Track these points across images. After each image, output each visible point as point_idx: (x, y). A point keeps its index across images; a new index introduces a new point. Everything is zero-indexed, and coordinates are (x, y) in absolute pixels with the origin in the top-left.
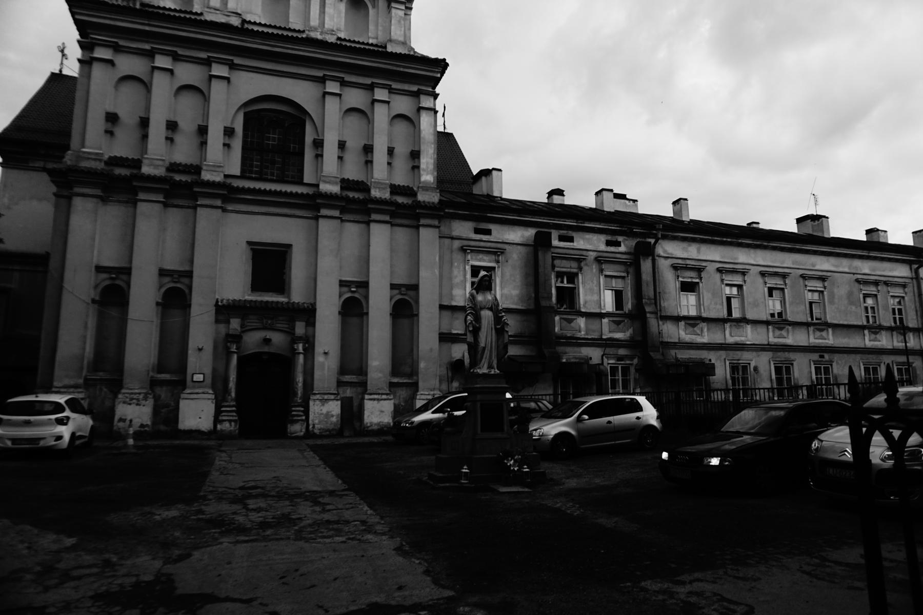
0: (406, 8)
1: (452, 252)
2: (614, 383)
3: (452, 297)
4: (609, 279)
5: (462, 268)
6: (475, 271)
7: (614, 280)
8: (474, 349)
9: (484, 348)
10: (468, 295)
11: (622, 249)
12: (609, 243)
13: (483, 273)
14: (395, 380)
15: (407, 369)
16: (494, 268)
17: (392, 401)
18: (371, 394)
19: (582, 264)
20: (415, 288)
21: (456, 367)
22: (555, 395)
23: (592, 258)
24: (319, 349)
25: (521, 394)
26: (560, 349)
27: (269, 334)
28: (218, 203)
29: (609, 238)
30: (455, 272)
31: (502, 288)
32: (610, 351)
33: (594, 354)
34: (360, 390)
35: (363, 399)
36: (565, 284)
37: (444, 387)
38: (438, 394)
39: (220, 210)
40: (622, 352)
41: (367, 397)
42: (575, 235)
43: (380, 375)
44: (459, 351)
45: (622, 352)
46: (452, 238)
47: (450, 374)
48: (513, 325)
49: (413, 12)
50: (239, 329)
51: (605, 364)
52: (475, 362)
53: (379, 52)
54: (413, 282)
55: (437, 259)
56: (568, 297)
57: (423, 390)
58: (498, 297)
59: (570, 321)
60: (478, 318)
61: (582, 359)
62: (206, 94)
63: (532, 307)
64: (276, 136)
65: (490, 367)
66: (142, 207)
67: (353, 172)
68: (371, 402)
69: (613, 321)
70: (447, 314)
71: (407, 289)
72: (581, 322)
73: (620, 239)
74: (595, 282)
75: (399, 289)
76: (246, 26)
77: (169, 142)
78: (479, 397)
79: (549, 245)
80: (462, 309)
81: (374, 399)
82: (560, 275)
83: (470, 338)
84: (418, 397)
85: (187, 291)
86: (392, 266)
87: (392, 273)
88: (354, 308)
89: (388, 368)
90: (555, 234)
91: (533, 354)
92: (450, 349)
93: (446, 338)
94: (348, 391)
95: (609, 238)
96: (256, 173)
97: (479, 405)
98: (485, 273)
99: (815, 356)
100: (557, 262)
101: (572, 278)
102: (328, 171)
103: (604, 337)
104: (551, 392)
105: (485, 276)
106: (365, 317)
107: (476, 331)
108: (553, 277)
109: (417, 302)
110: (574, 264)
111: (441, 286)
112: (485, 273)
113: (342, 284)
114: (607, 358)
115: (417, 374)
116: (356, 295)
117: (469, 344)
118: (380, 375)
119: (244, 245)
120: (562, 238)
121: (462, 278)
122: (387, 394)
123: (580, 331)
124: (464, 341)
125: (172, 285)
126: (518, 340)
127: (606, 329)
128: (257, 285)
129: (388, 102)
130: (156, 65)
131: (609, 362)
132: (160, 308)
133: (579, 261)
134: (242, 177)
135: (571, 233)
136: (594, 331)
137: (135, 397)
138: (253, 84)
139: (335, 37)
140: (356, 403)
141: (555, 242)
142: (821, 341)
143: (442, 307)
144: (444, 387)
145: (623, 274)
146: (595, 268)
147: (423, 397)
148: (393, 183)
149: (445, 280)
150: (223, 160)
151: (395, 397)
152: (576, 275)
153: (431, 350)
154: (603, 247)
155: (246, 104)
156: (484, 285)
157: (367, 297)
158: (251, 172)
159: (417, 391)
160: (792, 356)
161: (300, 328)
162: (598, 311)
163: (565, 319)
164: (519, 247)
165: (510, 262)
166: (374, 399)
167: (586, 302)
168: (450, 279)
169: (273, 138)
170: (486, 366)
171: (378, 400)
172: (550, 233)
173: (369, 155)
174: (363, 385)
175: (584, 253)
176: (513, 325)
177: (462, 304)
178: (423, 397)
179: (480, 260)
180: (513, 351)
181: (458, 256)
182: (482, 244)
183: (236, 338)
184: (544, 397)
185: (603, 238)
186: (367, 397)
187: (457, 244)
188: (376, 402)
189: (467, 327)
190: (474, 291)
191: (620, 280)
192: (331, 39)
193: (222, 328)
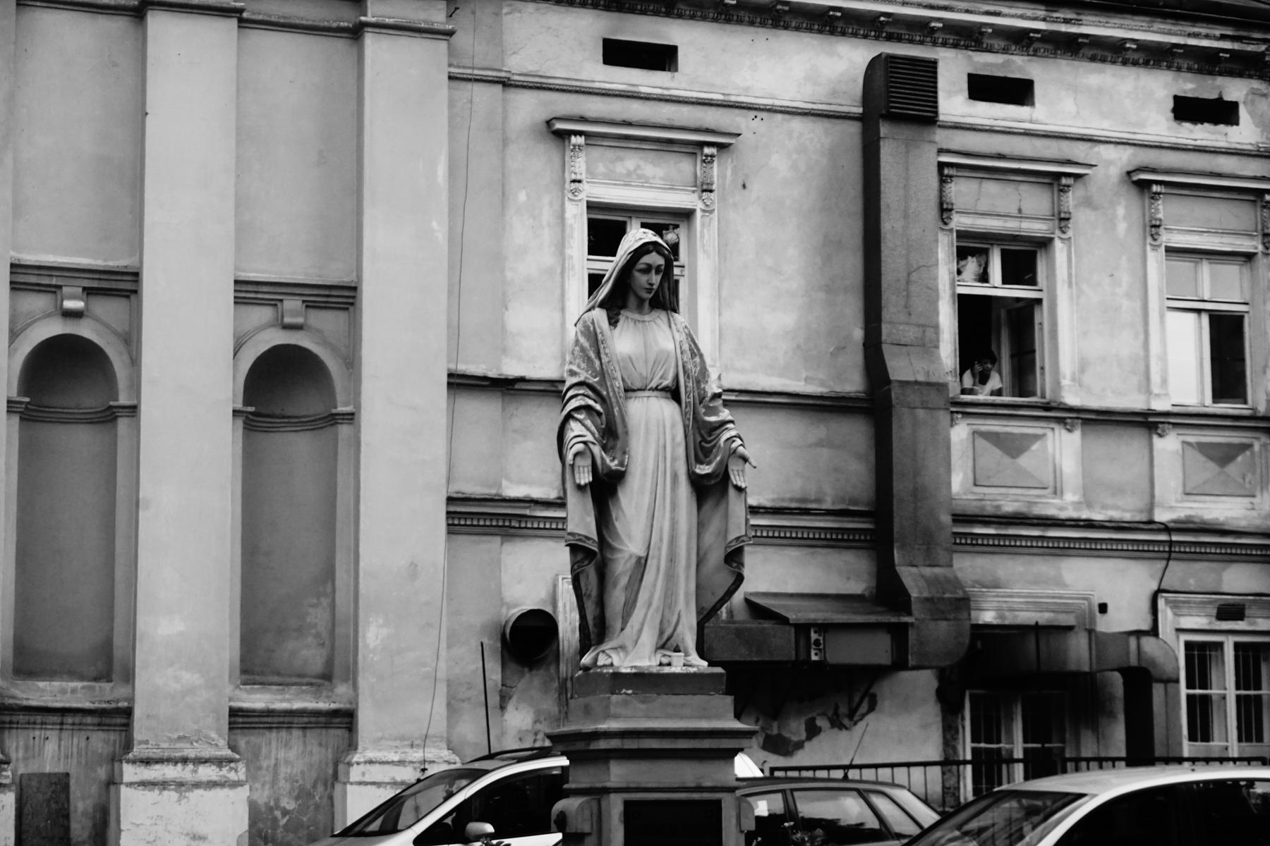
1: (505, 142)
2: (1201, 718)
3: (501, 341)
4: (1184, 266)
5: (547, 215)
6: (604, 234)
7: (1206, 269)
8: (592, 560)
9: (641, 564)
10: (572, 332)
11: (1244, 133)
12: (1186, 110)
13: (636, 236)
14: (257, 700)
15: (311, 656)
16: (686, 215)
17: (243, 793)
18: (147, 762)
19: (1071, 200)
20: (341, 298)
21: (527, 641)
22: (949, 763)
23: (1115, 172)
25: (800, 759)
26: (969, 567)
29: (1190, 86)
30: (519, 230)
31: (722, 302)
32: (1182, 574)
33: (1116, 591)
34: (100, 742)
35: (112, 782)
36: (997, 287)
37: (471, 730)
38: (441, 759)
39: (500, 87)
40: (1239, 579)
41: (130, 772)
42: (1045, 74)
43: (190, 678)
44: (535, 575)
45: (1239, 579)
46: (506, 84)
47: (495, 675)
48: (771, 461)
51: (1166, 629)
52: (595, 631)
54: (335, 274)
55: (442, 170)
56: (1001, 336)
57: (377, 742)
58: (706, 344)
59: (1013, 447)
60: (611, 434)
61: (1066, 609)
63: (853, 383)
65: (667, 644)
68: (151, 795)
69: (1202, 448)
70: (481, 409)
71: (309, 306)
72: (1063, 448)
73: (1234, 89)
74: (1125, 278)
75: (274, 304)
78: (618, 773)
79: (927, 118)
80: (551, 390)
81: (163, 785)
82: (971, 247)
83: (580, 518)
84: (355, 774)
86: (241, 203)
87: (243, 233)
89: (227, 650)
90: (953, 69)
91: (857, 587)
92: (497, 564)
93: (479, 517)
94: (51, 747)
95: (1190, 86)
97: (615, 806)
98: (650, 236)
100: (960, 191)
101: (1023, 259)
103: (1161, 516)
104: (932, 750)
105: (644, 249)
106: (123, 424)
107: (605, 488)
108: (944, 251)
109: (352, 362)
110: (1036, 200)
111: (455, 291)
112: (650, 236)
113: (248, 292)
114: (1175, 605)
115: (351, 675)
116: (85, 330)
117: (578, 550)
118: (190, 678)
120: (982, 88)
121: (548, 259)
122: (220, 762)
123: (1057, 491)
124: (554, 529)
125: (56, 328)
126: (791, 524)
127: (1172, 480)
128: (1220, 392)
131: (1184, 623)
132: (240, 423)
133: (1054, 182)
135: (1018, 65)
136: (1119, 490)
140: (81, 804)
141: (953, 102)
143: (460, 383)
144: (471, 730)
145: (1246, 245)
146: (1125, 213)
147: (377, 773)
149: (470, 261)
151: (252, 777)
152: (1045, 243)
153: (413, 570)
154: (1161, 126)
156: (639, 279)
157: (131, 339)
159: (352, 746)
162: (1133, 402)
163: (987, 436)
164: (797, 124)
165: (755, 187)
166: (163, 785)
167: (1083, 366)
168: (497, 260)
170: (649, 638)
171: (180, 785)
172: (932, 66)
174: (118, 718)
175: (1078, 151)
176: (771, 461)
177: (545, 369)
178: (377, 773)
179: (626, 181)
180: (773, 574)
181: (535, 161)
182: (636, 110)
184: (901, 774)
185: (1162, 86)
186: (130, 772)
187: (528, 109)
188: (171, 795)
189: (567, 469)
190: (600, 316)
191: (1231, 271)
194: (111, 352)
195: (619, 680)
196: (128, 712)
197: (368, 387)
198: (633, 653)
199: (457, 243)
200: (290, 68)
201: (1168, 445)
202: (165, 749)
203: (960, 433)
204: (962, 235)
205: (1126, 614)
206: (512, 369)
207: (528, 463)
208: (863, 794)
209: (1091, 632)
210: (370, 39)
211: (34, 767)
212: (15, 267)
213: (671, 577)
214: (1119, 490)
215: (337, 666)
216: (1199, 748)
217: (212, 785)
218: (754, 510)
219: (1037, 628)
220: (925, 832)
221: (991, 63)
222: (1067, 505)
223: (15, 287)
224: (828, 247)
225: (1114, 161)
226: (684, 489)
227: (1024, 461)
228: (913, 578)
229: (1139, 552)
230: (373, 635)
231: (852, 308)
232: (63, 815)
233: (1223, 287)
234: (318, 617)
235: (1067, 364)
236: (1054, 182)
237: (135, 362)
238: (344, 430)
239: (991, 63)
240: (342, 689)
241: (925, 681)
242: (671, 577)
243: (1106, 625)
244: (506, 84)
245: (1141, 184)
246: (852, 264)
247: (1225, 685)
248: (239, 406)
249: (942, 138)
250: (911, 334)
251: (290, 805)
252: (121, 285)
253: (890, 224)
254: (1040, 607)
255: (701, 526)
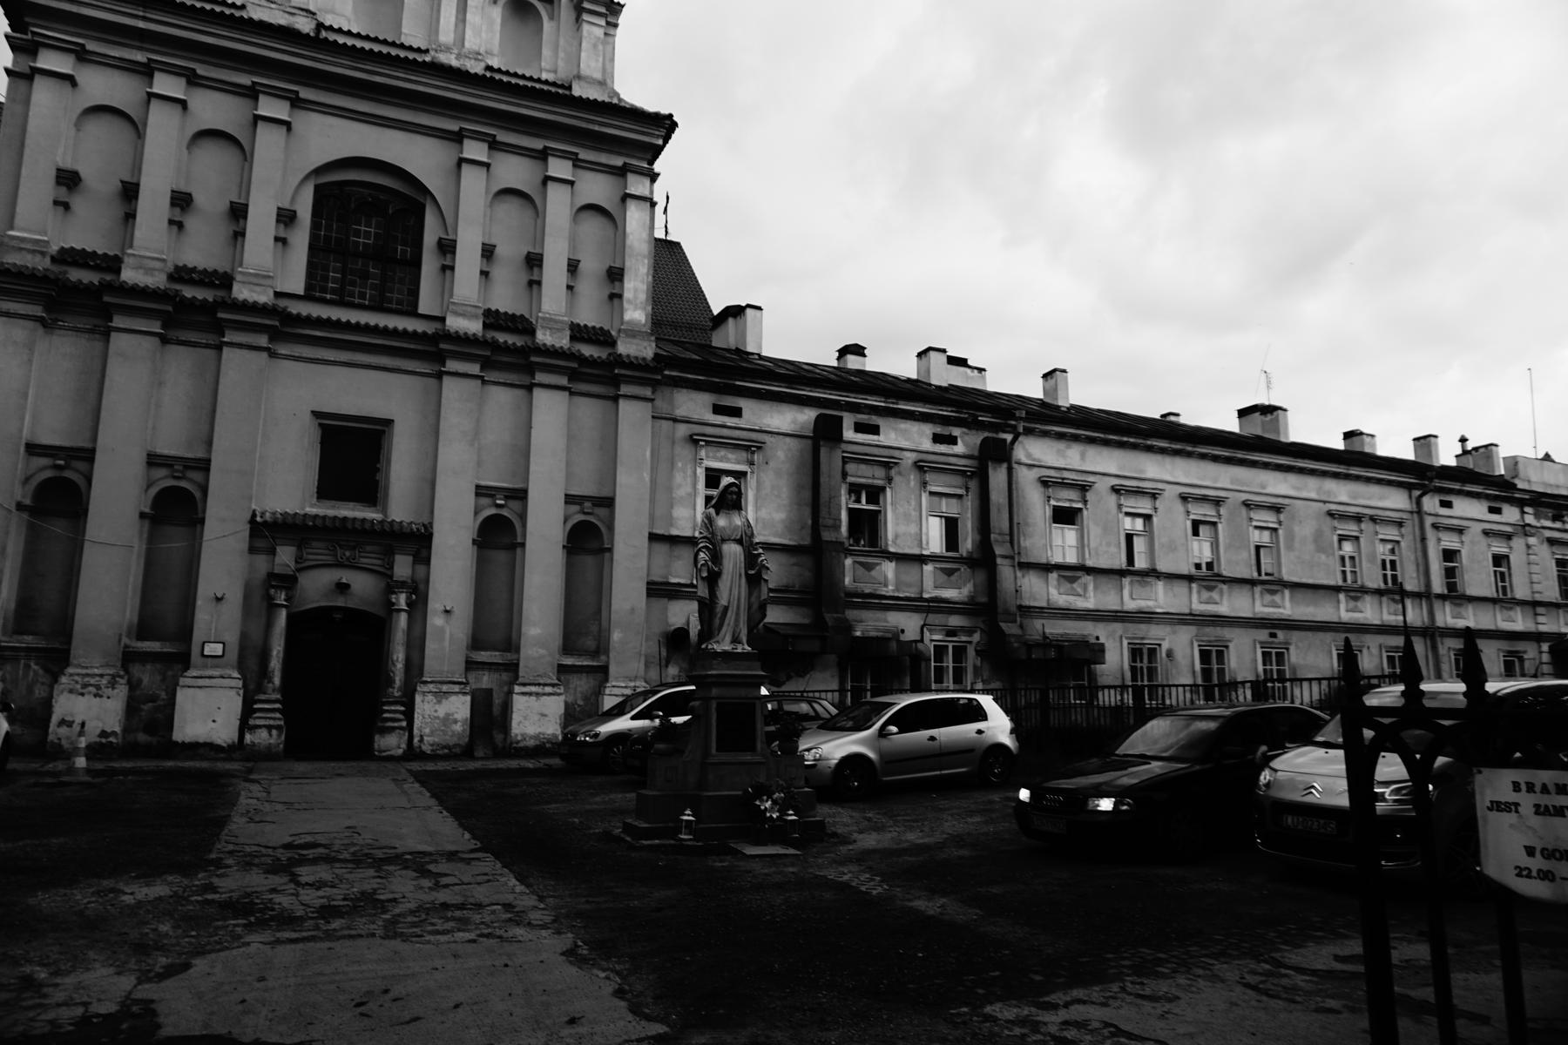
0: (608, 23)
2: (940, 672)
3: (670, 521)
4: (936, 499)
5: (689, 472)
6: (713, 477)
7: (944, 501)
8: (708, 609)
9: (726, 609)
11: (959, 448)
12: (937, 439)
13: (726, 481)
14: (569, 661)
15: (590, 644)
16: (744, 474)
18: (524, 685)
19: (893, 472)
20: (608, 502)
21: (676, 640)
22: (842, 691)
23: (910, 462)
24: (435, 605)
25: (784, 688)
26: (851, 614)
27: (346, 576)
28: (263, 341)
29: (939, 430)
30: (678, 478)
31: (757, 508)
33: (909, 625)
34: (505, 676)
35: (510, 692)
36: (864, 505)
37: (654, 674)
38: (642, 686)
40: (955, 621)
41: (517, 689)
43: (542, 651)
44: (683, 614)
45: (955, 621)
46: (675, 420)
47: (664, 653)
48: (776, 571)
49: (619, 31)
50: (292, 565)
51: (926, 640)
52: (707, 633)
53: (559, 95)
54: (605, 493)
55: (648, 454)
56: (867, 526)
57: (617, 679)
59: (869, 567)
60: (716, 557)
62: (247, 148)
64: (372, 232)
65: (736, 640)
66: (119, 342)
67: (505, 299)
68: (525, 698)
70: (662, 548)
72: (889, 569)
73: (956, 432)
76: (324, 34)
77: (175, 228)
78: (715, 692)
80: (691, 541)
81: (530, 694)
82: (855, 490)
83: (703, 591)
84: (607, 691)
85: (198, 495)
86: (568, 464)
87: (569, 476)
88: (499, 534)
89: (556, 641)
90: (848, 420)
91: (806, 621)
92: (666, 609)
93: (659, 590)
94: (485, 678)
95: (939, 430)
96: (333, 291)
97: (714, 705)
99: (1263, 635)
100: (851, 467)
101: (875, 494)
102: (462, 295)
103: (926, 596)
104: (835, 686)
106: (519, 550)
107: (713, 579)
108: (844, 491)
109: (611, 528)
110: (880, 472)
111: (652, 501)
113: (481, 491)
115: (607, 652)
116: (505, 512)
117: (701, 602)
118: (542, 651)
119: (308, 417)
120: (860, 428)
121: (689, 489)
122: (553, 685)
124: (691, 596)
125: (493, 511)
126: (783, 596)
127: (930, 583)
129: (572, 183)
130: (155, 90)
133: (887, 466)
134: (308, 297)
136: (910, 585)
137: (92, 681)
138: (332, 137)
139: (483, 65)
140: (497, 700)
141: (849, 434)
142: (1271, 610)
143: (653, 537)
144: (654, 674)
145: (959, 491)
146: (913, 479)
147: (616, 691)
148: (576, 321)
149: (660, 490)
150: (273, 266)
151: (566, 691)
152: (883, 489)
153: (633, 610)
154: (927, 445)
155: (318, 171)
156: (728, 500)
157: (523, 517)
158: (324, 290)
159: (607, 680)
160: (1227, 633)
161: (403, 567)
162: (916, 551)
163: (861, 564)
164: (788, 439)
165: (771, 464)
166: (530, 694)
167: (896, 536)
168: (670, 489)
169: (366, 233)
170: (728, 638)
171: (537, 694)
172: (841, 418)
173: (536, 270)
174: (512, 668)
175: (896, 453)
176: (776, 571)
177: (688, 533)
178: (616, 691)
180: (775, 615)
181: (684, 451)
183: (287, 581)
185: (928, 429)
186: (517, 689)
187: (683, 430)
189: (699, 571)
190: (712, 511)
191: (954, 501)
192: (476, 68)
193: (262, 563)
194: (603, 529)
195: (716, 654)
196: (517, 665)
197: (618, 538)
198: (723, 645)
199: (653, 481)
200: (589, 411)
201: (928, 568)
202: (532, 679)
203: (848, 562)
204: (851, 484)
205: (911, 634)
206: (675, 532)
207: (680, 571)
208: (810, 703)
209: (899, 641)
210: (622, 402)
211: (478, 686)
212: (478, 487)
213: (738, 614)
214: (910, 585)
215: (602, 648)
216: (939, 686)
217: (550, 694)
218: (771, 590)
219: (877, 638)
220: (833, 717)
221: (863, 418)
222: (890, 590)
223: (477, 494)
224: (798, 488)
225: (910, 457)
226: (744, 580)
227: (873, 573)
228: (829, 617)
229: (916, 610)
230: (616, 636)
231: (807, 511)
232: (490, 704)
233: (950, 508)
234: (594, 628)
235: (890, 536)
236: (887, 466)
237: (524, 525)
238: (607, 555)
239: (863, 418)
240: (603, 658)
241: (832, 658)
242: (738, 614)
243: (903, 638)
244: (675, 420)
245: (920, 467)
246: (807, 494)
247: (949, 663)
248: (147, 510)
249: (844, 446)
250: (830, 522)
251: (580, 702)
252: (520, 495)
253: (823, 479)
254: (878, 630)
255: (750, 594)
